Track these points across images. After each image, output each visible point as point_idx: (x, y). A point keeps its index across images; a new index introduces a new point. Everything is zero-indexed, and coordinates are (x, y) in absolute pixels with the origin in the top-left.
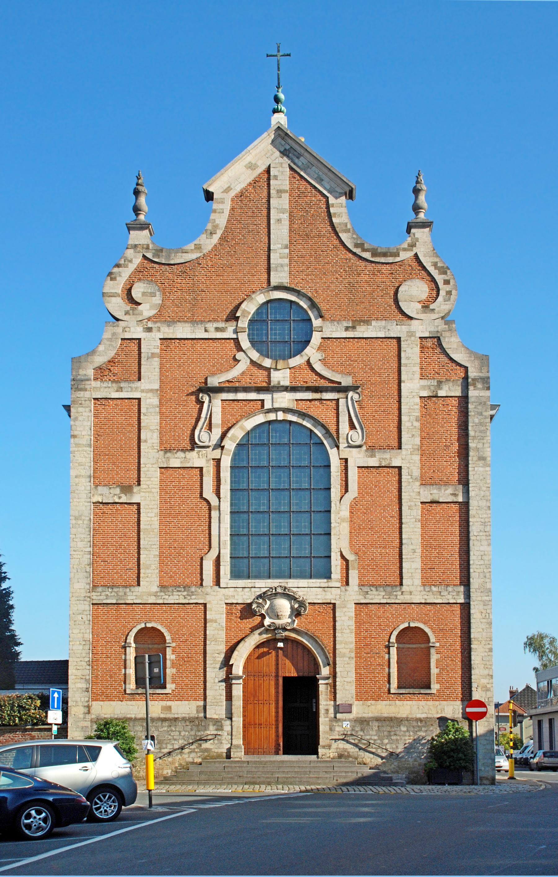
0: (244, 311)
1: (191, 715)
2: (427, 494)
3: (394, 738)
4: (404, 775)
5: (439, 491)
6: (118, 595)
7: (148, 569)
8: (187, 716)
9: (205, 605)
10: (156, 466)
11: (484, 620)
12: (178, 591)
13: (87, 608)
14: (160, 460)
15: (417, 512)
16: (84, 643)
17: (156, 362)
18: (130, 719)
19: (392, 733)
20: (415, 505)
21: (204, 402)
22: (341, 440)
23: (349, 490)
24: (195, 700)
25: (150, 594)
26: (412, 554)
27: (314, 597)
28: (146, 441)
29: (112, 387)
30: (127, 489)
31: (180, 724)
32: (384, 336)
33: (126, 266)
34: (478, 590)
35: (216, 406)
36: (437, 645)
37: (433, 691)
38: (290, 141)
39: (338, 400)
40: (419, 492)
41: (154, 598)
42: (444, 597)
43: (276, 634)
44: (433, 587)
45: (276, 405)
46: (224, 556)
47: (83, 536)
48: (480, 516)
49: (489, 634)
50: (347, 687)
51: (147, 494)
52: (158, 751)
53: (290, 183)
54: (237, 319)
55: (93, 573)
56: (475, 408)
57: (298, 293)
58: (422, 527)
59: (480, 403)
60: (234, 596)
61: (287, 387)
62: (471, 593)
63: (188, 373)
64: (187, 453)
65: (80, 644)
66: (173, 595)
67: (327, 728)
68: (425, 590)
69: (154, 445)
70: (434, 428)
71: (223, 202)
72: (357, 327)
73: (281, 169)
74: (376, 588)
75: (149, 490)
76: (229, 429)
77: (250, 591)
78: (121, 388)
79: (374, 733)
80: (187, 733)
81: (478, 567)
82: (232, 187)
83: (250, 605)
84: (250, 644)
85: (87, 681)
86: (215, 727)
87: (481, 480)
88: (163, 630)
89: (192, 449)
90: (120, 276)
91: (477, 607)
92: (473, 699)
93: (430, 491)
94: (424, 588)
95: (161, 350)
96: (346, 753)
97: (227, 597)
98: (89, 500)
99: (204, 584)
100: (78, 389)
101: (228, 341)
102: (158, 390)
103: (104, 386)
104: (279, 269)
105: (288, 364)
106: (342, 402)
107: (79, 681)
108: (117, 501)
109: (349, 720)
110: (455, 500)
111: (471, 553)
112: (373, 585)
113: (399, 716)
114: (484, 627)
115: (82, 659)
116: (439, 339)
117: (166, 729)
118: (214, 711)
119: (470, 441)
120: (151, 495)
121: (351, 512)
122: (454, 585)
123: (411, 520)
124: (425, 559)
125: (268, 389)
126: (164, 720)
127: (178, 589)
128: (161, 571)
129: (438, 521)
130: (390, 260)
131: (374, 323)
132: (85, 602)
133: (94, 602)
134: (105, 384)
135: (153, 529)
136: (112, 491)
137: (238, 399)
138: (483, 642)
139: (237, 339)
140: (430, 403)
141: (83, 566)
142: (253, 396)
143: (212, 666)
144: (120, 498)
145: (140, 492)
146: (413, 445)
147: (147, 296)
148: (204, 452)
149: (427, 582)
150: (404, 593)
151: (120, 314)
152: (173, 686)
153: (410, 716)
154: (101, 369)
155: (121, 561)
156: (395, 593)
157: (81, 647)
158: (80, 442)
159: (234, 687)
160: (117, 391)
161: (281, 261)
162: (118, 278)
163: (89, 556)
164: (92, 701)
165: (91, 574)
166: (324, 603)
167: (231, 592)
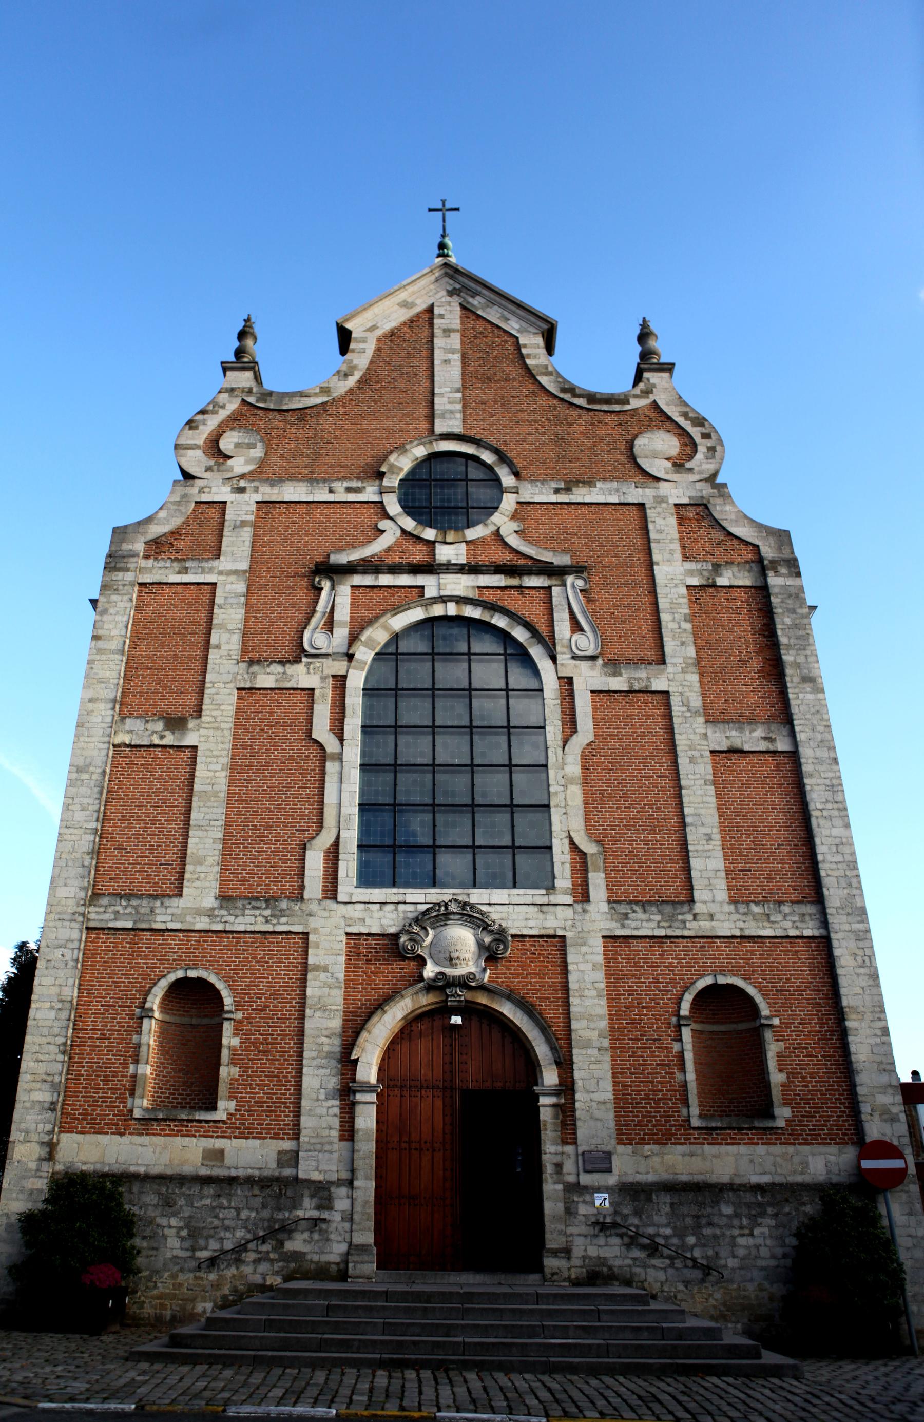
0: (392, 466)
1: (266, 1173)
2: (720, 738)
3: (707, 1231)
4: (739, 1326)
5: (741, 732)
6: (137, 913)
7: (200, 864)
8: (257, 1173)
9: (306, 935)
10: (232, 685)
11: (862, 971)
12: (254, 908)
13: (75, 935)
14: (239, 677)
15: (705, 768)
16: (60, 1006)
17: (247, 534)
18: (136, 1176)
19: (704, 1221)
20: (702, 756)
21: (322, 589)
22: (558, 648)
23: (579, 729)
24: (276, 1137)
25: (199, 912)
26: (705, 842)
27: (522, 924)
28: (218, 647)
29: (172, 567)
30: (176, 723)
31: (239, 1192)
32: (617, 501)
33: (216, 413)
34: (840, 911)
35: (340, 598)
36: (776, 1021)
37: (781, 1123)
38: (461, 278)
39: (550, 588)
40: (705, 735)
41: (207, 920)
42: (777, 925)
43: (448, 996)
44: (752, 905)
45: (444, 593)
46: (346, 842)
47: (86, 801)
48: (823, 775)
49: (876, 998)
50: (598, 1114)
51: (211, 732)
52: (188, 1254)
53: (462, 323)
54: (381, 476)
55: (96, 870)
56: (782, 602)
57: (477, 442)
58: (718, 795)
59: (790, 596)
60: (364, 920)
61: (463, 565)
62: (829, 917)
63: (299, 549)
64: (288, 666)
65: (52, 1008)
66: (243, 915)
67: (561, 1206)
68: (737, 912)
69: (231, 653)
70: (717, 633)
71: (364, 342)
72: (574, 489)
73: (448, 308)
74: (643, 906)
75: (216, 725)
76: (362, 628)
77: (396, 909)
78: (187, 569)
79: (663, 1220)
80: (253, 1214)
81: (834, 866)
82: (378, 325)
83: (396, 937)
84: (394, 1018)
85: (54, 1086)
86: (315, 1201)
87: (813, 714)
88: (220, 985)
89: (297, 660)
90: (204, 424)
91: (844, 943)
92: (868, 1140)
93: (725, 732)
94: (736, 907)
95: (257, 517)
96: (605, 1269)
97: (349, 921)
98: (106, 739)
99: (306, 896)
100: (116, 569)
101: (366, 506)
102: (246, 571)
103: (159, 565)
104: (447, 415)
105: (464, 536)
106: (556, 591)
107: (38, 1085)
108: (157, 741)
109: (607, 1189)
110: (772, 748)
111: (818, 841)
112: (637, 902)
113: (713, 1179)
114: (864, 984)
115: (50, 1039)
116: (706, 506)
117: (208, 1201)
118: (314, 1164)
119: (782, 652)
120: (219, 733)
121: (584, 768)
122: (792, 902)
123: (697, 782)
124: (729, 852)
125: (430, 568)
126: (207, 1181)
127: (254, 903)
128: (224, 870)
129: (747, 785)
130: (617, 408)
131: (599, 484)
132: (74, 924)
133: (92, 924)
134: (161, 564)
135: (217, 792)
136: (150, 726)
137: (380, 584)
138: (868, 1016)
139: (381, 502)
140: (705, 596)
141: (78, 855)
142: (405, 580)
143: (315, 1063)
144: (162, 737)
145: (199, 727)
146: (684, 658)
147: (242, 447)
148: (318, 665)
149: (739, 897)
150: (698, 917)
151: (197, 469)
152: (232, 1105)
153: (737, 1181)
154: (157, 543)
155: (151, 849)
156: (680, 917)
157: (52, 1014)
158: (105, 647)
159: (359, 1109)
160: (179, 573)
161: (449, 407)
162: (201, 427)
163: (92, 838)
164: (60, 1132)
165: (93, 872)
166: (541, 936)
167: (356, 912)
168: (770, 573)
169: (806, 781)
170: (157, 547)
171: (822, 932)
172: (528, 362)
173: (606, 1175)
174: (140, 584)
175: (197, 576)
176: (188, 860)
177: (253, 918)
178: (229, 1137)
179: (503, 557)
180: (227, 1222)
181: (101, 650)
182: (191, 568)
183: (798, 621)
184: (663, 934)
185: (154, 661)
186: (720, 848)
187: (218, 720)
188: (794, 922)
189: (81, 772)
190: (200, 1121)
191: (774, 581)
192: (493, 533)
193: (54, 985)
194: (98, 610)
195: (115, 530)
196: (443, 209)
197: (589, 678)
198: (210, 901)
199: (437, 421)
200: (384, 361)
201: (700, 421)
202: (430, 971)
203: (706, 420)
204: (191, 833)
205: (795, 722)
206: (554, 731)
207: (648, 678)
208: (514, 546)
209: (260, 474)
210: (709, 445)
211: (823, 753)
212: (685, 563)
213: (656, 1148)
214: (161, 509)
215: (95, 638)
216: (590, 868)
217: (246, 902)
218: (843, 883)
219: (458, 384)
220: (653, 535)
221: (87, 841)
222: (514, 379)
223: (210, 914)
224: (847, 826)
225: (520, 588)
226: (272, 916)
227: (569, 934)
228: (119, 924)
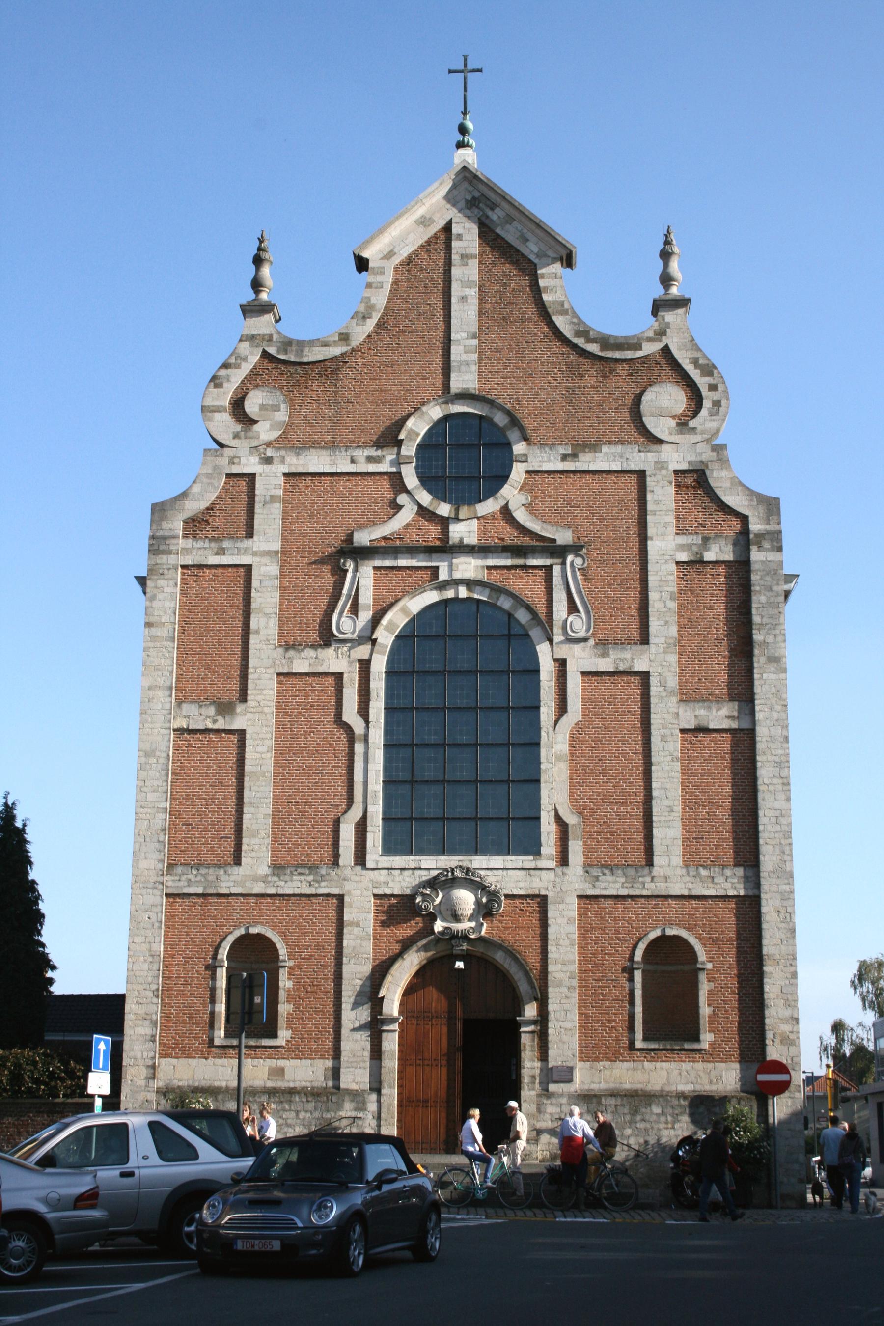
2: (689, 717)
6: (206, 880)
7: (254, 836)
8: (309, 1084)
10: (272, 671)
11: (783, 925)
14: (278, 662)
16: (150, 959)
17: (277, 509)
20: (672, 734)
25: (256, 879)
26: (667, 814)
28: (257, 632)
30: (225, 708)
31: (297, 1099)
34: (772, 875)
35: (364, 578)
36: (709, 966)
37: (705, 1045)
39: (551, 566)
40: (677, 714)
41: (262, 884)
44: (701, 869)
47: (156, 783)
48: (773, 753)
49: (790, 948)
54: (399, 444)
56: (761, 579)
58: (683, 771)
60: (388, 883)
62: (762, 879)
64: (319, 650)
66: (292, 880)
69: (269, 638)
72: (580, 455)
74: (612, 870)
75: (259, 709)
78: (224, 549)
80: (308, 1115)
83: (412, 897)
89: (327, 644)
90: (228, 381)
92: (768, 1059)
93: (694, 711)
98: (167, 725)
103: (199, 546)
105: (476, 512)
106: (557, 570)
108: (210, 726)
111: (761, 813)
114: (783, 936)
123: (665, 759)
124: (686, 821)
126: (272, 1092)
127: (299, 870)
130: (629, 354)
132: (156, 892)
133: (170, 891)
134: (200, 544)
136: (203, 711)
144: (215, 721)
146: (666, 637)
147: (267, 409)
150: (655, 879)
151: (226, 436)
156: (641, 879)
160: (217, 554)
161: (465, 357)
162: (225, 385)
168: (754, 548)
169: (758, 758)
170: (196, 525)
171: (731, 883)
172: (546, 297)
173: (567, 1085)
174: (183, 567)
175: (234, 557)
176: (244, 833)
177: (299, 883)
178: (287, 1059)
179: (510, 536)
180: (289, 1121)
181: (155, 637)
182: (228, 548)
183: (772, 599)
184: (626, 893)
185: (201, 647)
186: (679, 819)
187: (262, 704)
188: (733, 883)
189: (149, 756)
190: (265, 1047)
191: (757, 556)
192: (502, 508)
193: (145, 942)
194: (148, 595)
195: (153, 505)
196: (465, 70)
197: (580, 659)
198: (264, 870)
199: (453, 376)
200: (401, 298)
201: (708, 370)
202: (439, 926)
203: (715, 368)
204: (245, 810)
205: (757, 702)
206: (547, 712)
207: (632, 659)
208: (521, 522)
209: (287, 441)
210: (715, 399)
211: (778, 731)
212: (677, 537)
213: (607, 1064)
214: (194, 482)
215: (148, 625)
216: (570, 837)
217: (293, 869)
218: (777, 851)
219: (475, 329)
220: (650, 507)
221: (161, 819)
222: (530, 319)
223: (264, 879)
224: (788, 799)
225: (525, 567)
226: (314, 880)
227: (550, 894)
228: (191, 890)
